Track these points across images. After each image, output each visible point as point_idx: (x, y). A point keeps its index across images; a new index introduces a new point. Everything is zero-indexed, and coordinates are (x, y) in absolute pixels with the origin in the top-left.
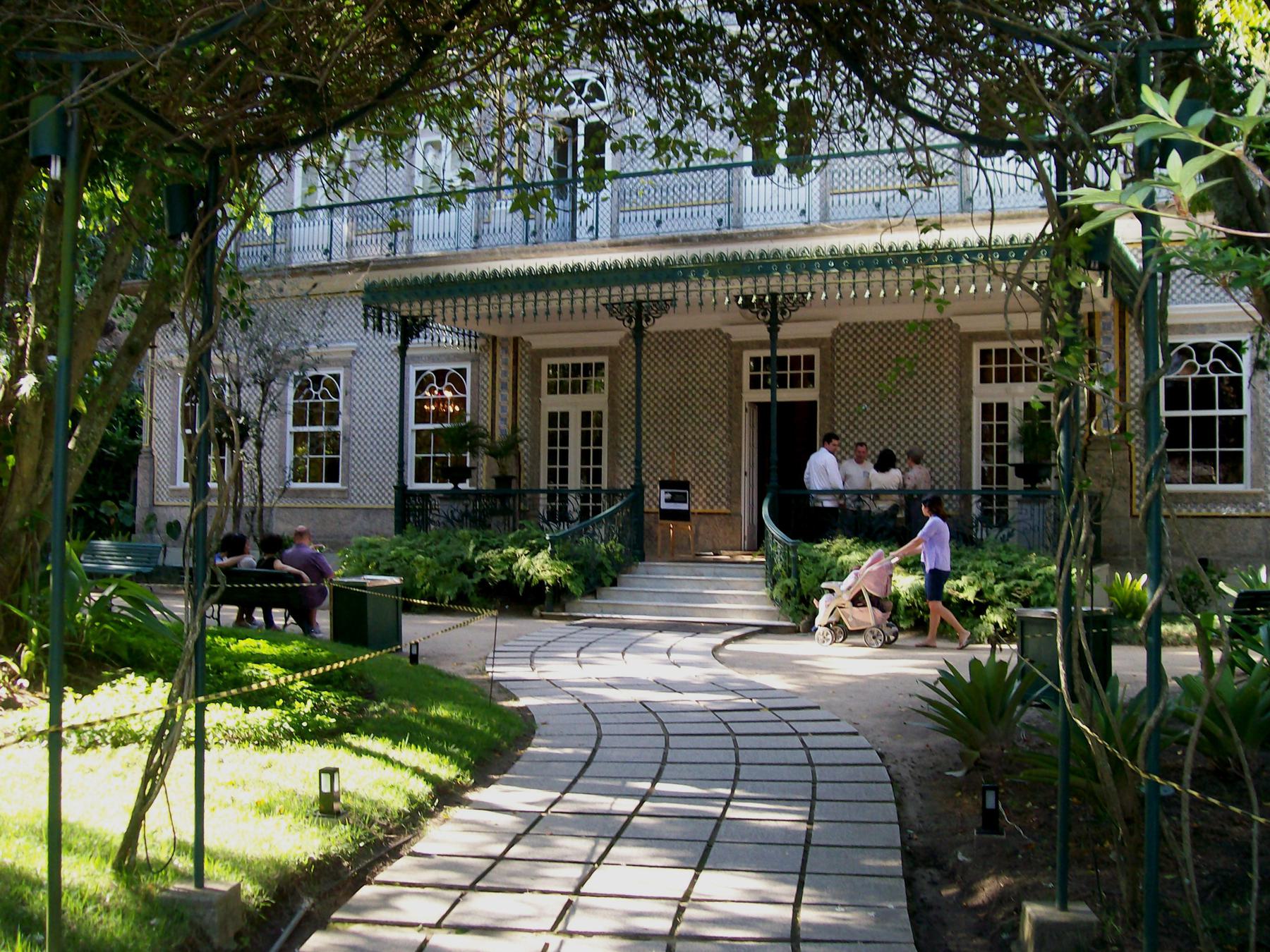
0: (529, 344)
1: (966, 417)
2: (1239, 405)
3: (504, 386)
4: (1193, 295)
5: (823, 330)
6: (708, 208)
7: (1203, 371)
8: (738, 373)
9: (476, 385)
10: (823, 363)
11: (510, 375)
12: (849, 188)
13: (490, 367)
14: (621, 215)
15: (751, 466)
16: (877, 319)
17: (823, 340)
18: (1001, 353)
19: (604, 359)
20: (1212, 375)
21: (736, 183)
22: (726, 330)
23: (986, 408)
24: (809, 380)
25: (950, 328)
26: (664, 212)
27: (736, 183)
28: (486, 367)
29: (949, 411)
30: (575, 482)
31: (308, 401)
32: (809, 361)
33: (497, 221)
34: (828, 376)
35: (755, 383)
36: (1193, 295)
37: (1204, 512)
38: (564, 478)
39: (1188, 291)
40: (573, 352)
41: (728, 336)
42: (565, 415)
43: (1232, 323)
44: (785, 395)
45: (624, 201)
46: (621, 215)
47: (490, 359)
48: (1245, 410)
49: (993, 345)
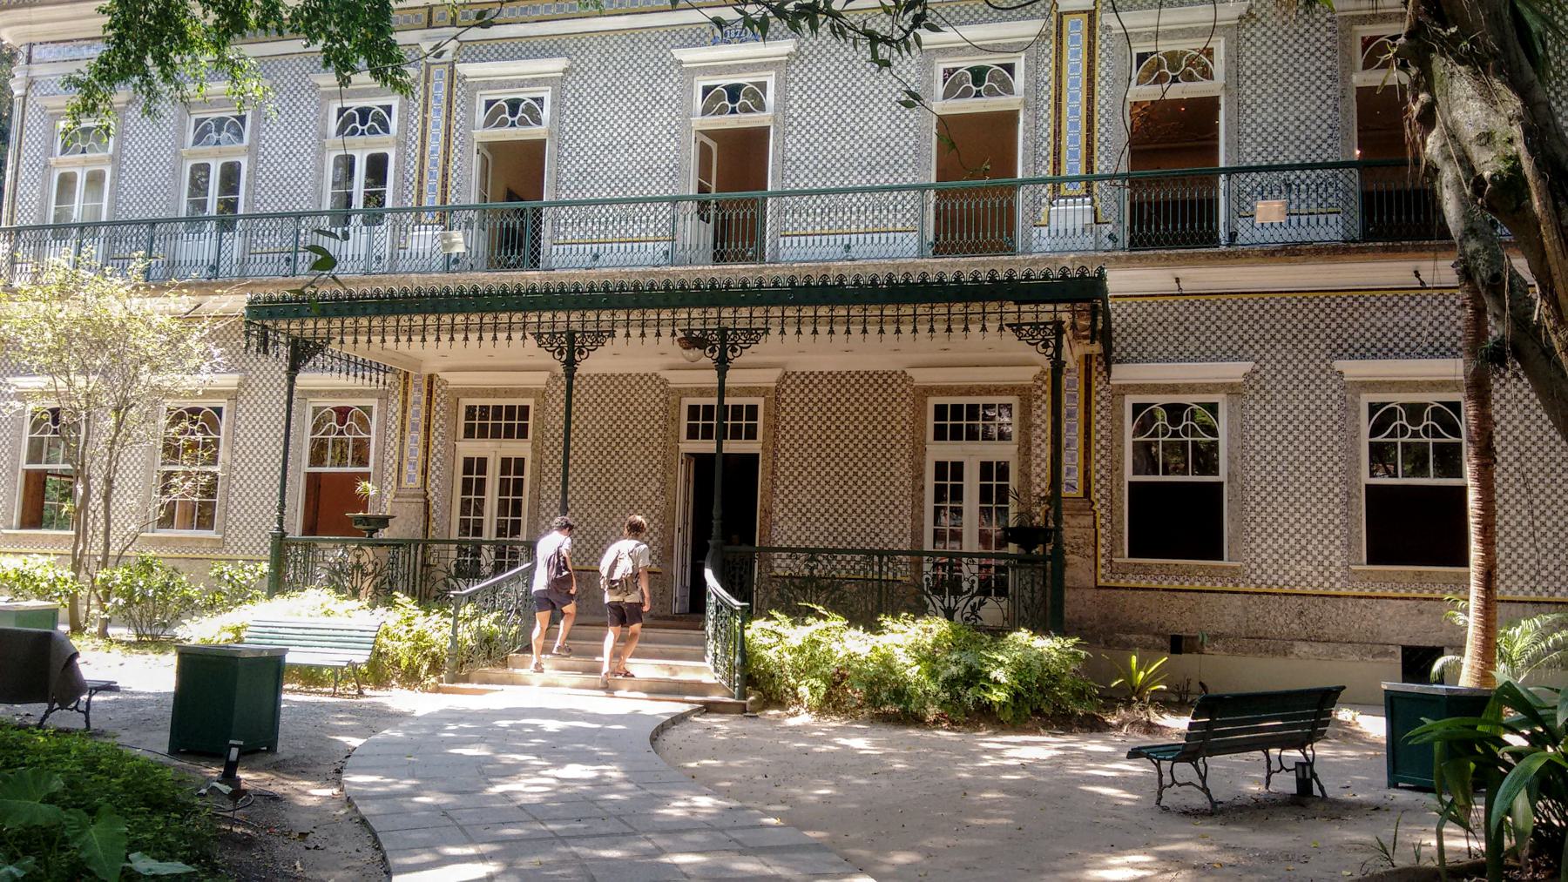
0: (446, 383)
1: (919, 476)
2: (366, 464)
3: (415, 427)
4: (1165, 354)
5: (769, 378)
6: (650, 245)
7: (1175, 434)
8: (676, 420)
9: (384, 425)
10: (767, 414)
11: (423, 414)
12: (809, 230)
13: (400, 406)
14: (555, 248)
15: (685, 523)
16: (862, 368)
17: (768, 389)
18: (957, 409)
19: (1013, 400)
20: (1425, 439)
21: (681, 218)
22: (664, 374)
23: (940, 468)
24: (523, 433)
25: (904, 381)
26: (854, 237)
27: (681, 218)
28: (396, 406)
29: (902, 470)
30: (489, 532)
31: (1399, 440)
32: (752, 411)
33: (415, 247)
34: (773, 427)
35: (692, 434)
36: (1165, 354)
37: (1176, 585)
38: (478, 531)
39: (1160, 349)
40: (495, 393)
41: (665, 382)
42: (483, 462)
43: (1208, 384)
44: (733, 447)
45: (559, 233)
46: (555, 248)
47: (400, 397)
48: (1222, 477)
49: (949, 401)
